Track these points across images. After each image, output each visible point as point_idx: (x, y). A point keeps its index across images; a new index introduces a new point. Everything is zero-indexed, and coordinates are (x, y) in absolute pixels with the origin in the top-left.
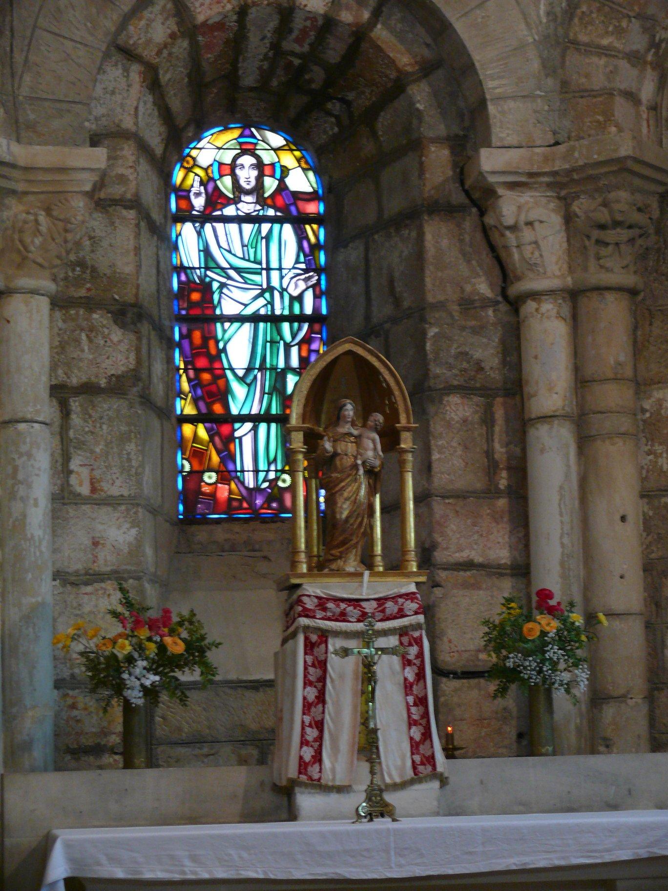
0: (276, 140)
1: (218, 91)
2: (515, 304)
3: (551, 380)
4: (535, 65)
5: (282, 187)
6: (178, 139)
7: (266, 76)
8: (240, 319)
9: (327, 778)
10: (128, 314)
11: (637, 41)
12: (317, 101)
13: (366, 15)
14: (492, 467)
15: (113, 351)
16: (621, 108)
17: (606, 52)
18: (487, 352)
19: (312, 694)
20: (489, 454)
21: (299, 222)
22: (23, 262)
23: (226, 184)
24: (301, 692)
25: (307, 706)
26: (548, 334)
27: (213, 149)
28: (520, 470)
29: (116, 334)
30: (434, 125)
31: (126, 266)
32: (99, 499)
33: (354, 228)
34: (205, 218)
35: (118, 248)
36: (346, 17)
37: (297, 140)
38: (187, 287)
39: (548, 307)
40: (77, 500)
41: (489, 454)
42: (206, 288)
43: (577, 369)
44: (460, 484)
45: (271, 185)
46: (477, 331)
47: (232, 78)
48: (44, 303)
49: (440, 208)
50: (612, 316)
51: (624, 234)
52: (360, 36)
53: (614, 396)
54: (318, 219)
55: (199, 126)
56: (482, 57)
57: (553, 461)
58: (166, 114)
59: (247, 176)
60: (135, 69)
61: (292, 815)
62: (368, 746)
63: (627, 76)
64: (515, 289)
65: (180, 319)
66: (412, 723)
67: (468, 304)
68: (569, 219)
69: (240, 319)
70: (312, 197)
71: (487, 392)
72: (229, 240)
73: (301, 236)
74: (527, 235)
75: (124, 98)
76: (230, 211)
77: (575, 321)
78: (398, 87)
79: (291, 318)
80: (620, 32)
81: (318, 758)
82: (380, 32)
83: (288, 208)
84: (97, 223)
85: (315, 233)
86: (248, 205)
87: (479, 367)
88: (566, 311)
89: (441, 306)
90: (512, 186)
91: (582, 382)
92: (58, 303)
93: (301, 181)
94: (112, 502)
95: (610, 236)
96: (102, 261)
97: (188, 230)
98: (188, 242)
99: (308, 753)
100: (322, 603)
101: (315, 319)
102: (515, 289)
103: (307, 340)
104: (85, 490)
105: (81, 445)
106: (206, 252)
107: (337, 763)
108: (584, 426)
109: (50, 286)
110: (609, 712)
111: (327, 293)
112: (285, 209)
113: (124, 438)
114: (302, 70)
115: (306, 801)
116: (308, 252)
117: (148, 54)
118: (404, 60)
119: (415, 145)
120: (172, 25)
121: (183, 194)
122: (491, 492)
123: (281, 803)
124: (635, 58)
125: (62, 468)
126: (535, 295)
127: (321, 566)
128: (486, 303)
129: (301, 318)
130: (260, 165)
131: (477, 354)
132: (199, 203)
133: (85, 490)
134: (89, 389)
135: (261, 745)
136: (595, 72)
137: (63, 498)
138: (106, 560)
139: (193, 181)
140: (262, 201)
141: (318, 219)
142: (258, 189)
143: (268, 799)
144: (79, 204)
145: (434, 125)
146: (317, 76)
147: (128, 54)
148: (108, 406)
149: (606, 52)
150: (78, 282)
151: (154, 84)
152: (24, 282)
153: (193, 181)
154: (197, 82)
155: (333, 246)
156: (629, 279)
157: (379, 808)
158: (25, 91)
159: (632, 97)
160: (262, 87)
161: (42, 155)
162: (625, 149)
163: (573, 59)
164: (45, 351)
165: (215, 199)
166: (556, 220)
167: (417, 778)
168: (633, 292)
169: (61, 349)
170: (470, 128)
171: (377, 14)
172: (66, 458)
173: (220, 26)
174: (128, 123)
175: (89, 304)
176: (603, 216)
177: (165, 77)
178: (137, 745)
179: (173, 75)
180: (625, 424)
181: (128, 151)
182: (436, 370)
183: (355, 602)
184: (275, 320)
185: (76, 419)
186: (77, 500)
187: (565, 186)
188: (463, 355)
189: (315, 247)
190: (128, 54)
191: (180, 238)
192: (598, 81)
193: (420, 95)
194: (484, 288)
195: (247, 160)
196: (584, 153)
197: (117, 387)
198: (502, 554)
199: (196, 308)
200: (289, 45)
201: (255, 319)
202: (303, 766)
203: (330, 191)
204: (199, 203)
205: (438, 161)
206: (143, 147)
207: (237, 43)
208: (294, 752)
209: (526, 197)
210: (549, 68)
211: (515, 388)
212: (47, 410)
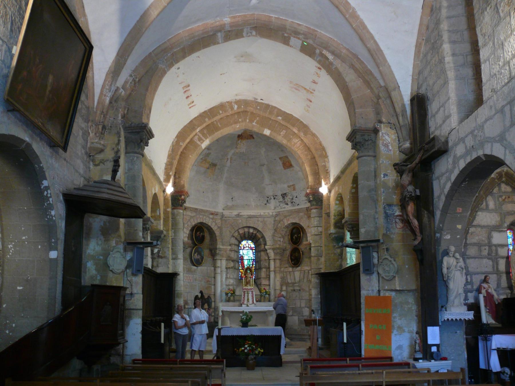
6: (240, 242)
10: (233, 261)
11: (280, 236)
15: (232, 264)
16: (279, 243)
18: (267, 264)
21: (252, 250)
22: (223, 257)
24: (243, 296)
26: (272, 263)
27: (244, 243)
28: (269, 275)
32: (230, 278)
33: (258, 250)
35: (233, 255)
37: (252, 242)
49: (263, 251)
50: (278, 262)
52: (256, 234)
53: (277, 269)
56: (266, 237)
57: (272, 275)
58: (238, 241)
62: (248, 300)
63: (279, 239)
67: (265, 260)
75: (233, 241)
77: (275, 262)
78: (259, 239)
82: (257, 234)
83: (251, 249)
84: (230, 252)
85: (254, 251)
86: (247, 248)
91: (275, 268)
92: (226, 260)
93: (253, 246)
98: (241, 252)
107: (246, 302)
108: (275, 271)
119: (261, 244)
122: (267, 278)
124: (280, 237)
125: (227, 275)
127: (246, 285)
134: (229, 268)
135: (240, 301)
136: (276, 239)
137: (227, 278)
138: (230, 284)
139: (242, 246)
147: (234, 237)
148: (231, 269)
151: (236, 239)
153: (242, 246)
154: (241, 237)
155: (255, 252)
157: (248, 306)
161: (225, 247)
165: (244, 248)
169: (227, 264)
170: (265, 244)
178: (228, 300)
181: (233, 246)
187: (274, 249)
190: (234, 237)
191: (442, 109)
193: (261, 240)
194: (267, 258)
196: (275, 247)
197: (232, 268)
199: (242, 259)
205: (263, 246)
206: (235, 245)
208: (242, 301)
210: (273, 238)
211: (269, 268)
212: (225, 270)
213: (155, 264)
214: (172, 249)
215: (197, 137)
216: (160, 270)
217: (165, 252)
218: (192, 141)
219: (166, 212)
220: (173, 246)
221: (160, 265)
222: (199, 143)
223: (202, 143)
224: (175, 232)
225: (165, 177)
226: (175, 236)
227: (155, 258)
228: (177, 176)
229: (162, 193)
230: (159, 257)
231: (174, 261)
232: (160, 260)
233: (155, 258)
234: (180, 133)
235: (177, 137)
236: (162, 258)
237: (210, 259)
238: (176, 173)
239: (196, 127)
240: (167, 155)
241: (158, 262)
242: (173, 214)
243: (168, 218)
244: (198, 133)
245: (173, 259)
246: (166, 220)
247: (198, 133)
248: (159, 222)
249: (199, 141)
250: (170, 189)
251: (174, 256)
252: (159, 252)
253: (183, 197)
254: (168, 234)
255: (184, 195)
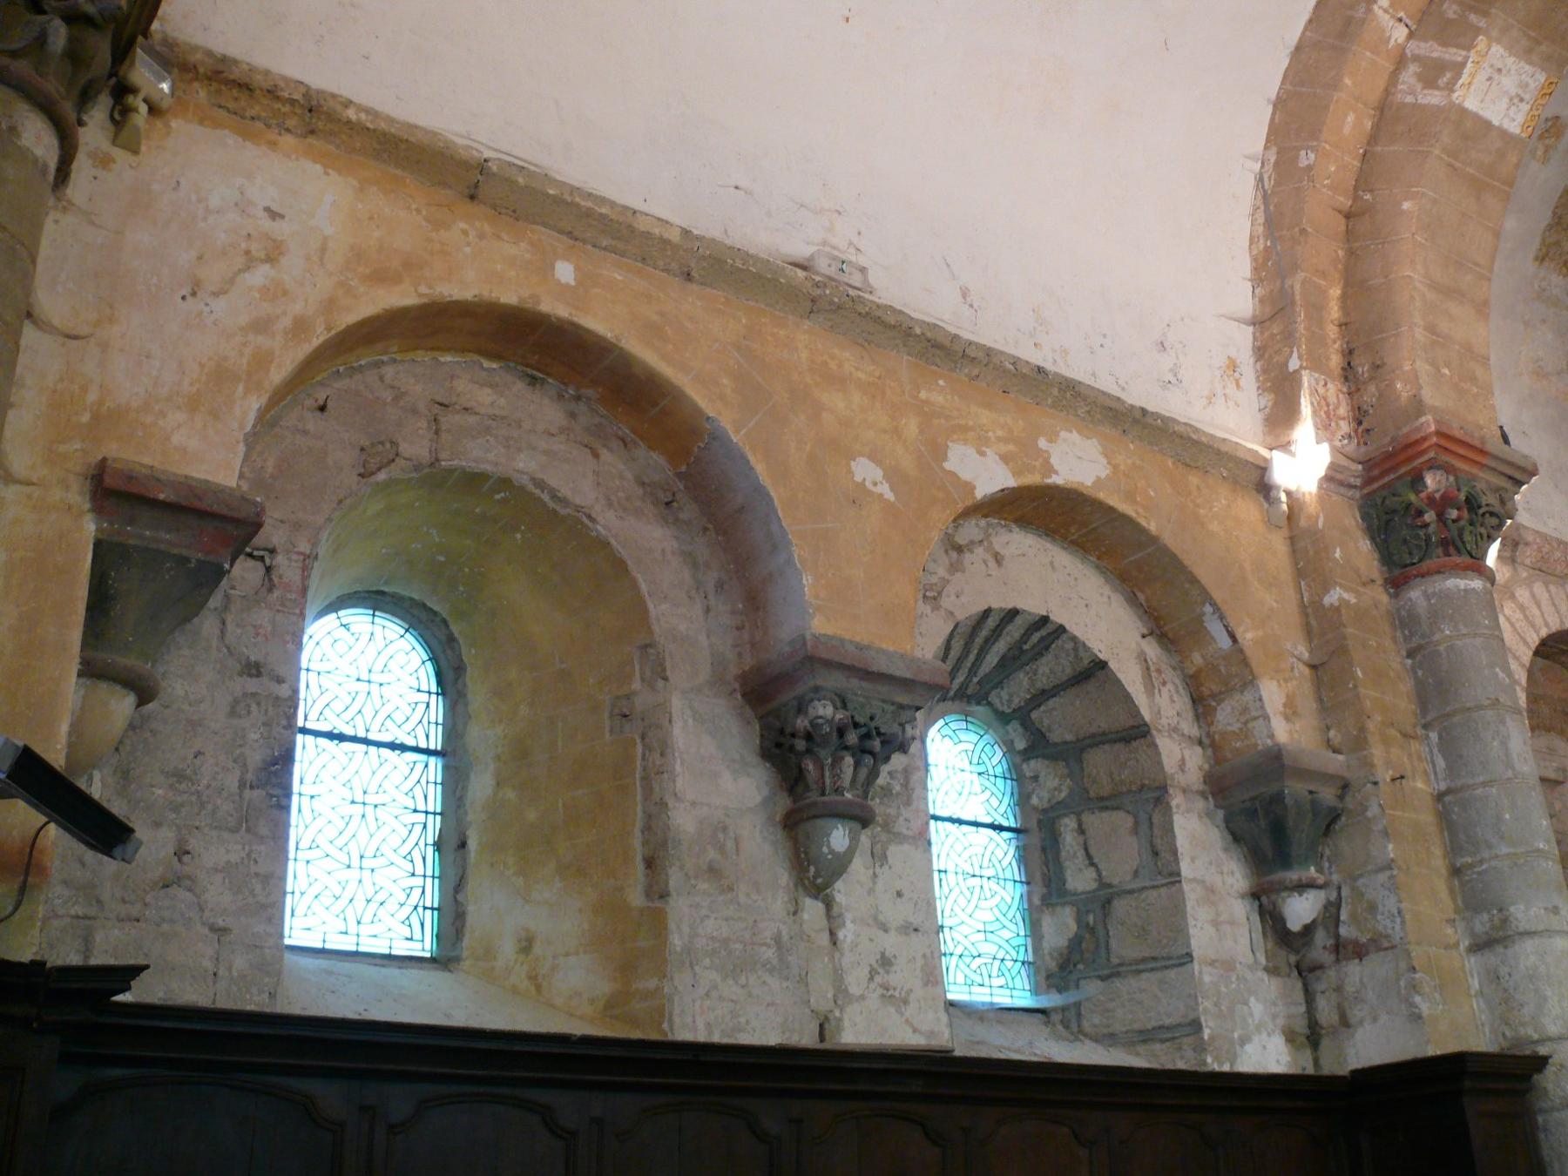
53: (827, 249)
213: (1326, 1011)
214: (1456, 871)
215: (1409, 76)
216: (1372, 1045)
217: (1372, 908)
218: (1388, 116)
219: (1320, 625)
220: (1454, 848)
221: (1356, 1014)
222: (1433, 98)
223: (1450, 87)
224: (1448, 746)
225: (1267, 400)
226: (1451, 770)
227: (1318, 967)
228: (1363, 369)
229: (1248, 509)
230: (1340, 949)
231: (1491, 958)
232: (1354, 972)
233: (1318, 967)
234: (1279, 104)
235: (1276, 134)
236: (1359, 951)
237: (1069, 671)
238: (1349, 353)
239: (1360, 12)
240: (1246, 267)
241: (1339, 989)
242: (1405, 622)
243: (1341, 650)
244: (1414, 47)
245: (1481, 945)
246: (1328, 672)
247: (1414, 47)
248: (1248, 696)
249: (1429, 82)
250: (1304, 464)
251: (1482, 923)
252: (1331, 912)
253: (1431, 481)
254: (1368, 764)
255: (1432, 466)
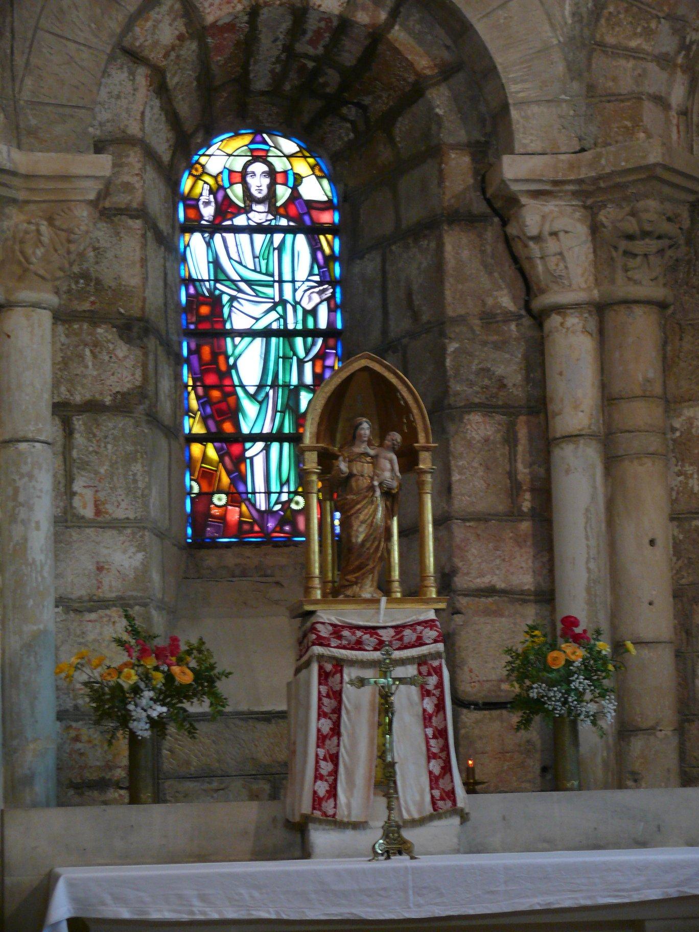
0: (289, 146)
1: (228, 95)
2: (539, 318)
3: (576, 397)
4: (560, 68)
5: (295, 195)
6: (187, 146)
7: (278, 80)
8: (252, 334)
9: (342, 814)
10: (134, 329)
11: (666, 43)
12: (332, 106)
13: (383, 16)
14: (515, 489)
15: (118, 368)
17: (634, 54)
18: (509, 368)
19: (326, 725)
20: (512, 474)
21: (313, 232)
22: (24, 274)
23: (236, 193)
24: (315, 724)
25: (322, 739)
26: (574, 349)
27: (223, 155)
28: (544, 492)
29: (122, 350)
30: (454, 131)
31: (131, 278)
32: (104, 522)
33: (371, 238)
34: (214, 228)
35: (124, 259)
36: (362, 18)
37: (311, 146)
38: (195, 300)
39: (573, 321)
40: (81, 523)
41: (512, 474)
42: (215, 301)
43: (604, 386)
44: (482, 507)
45: (283, 194)
46: (499, 346)
47: (242, 81)
48: (46, 317)
49: (461, 218)
50: (641, 331)
51: (653, 245)
52: (376, 37)
53: (642, 414)
54: (332, 230)
55: (209, 132)
56: (504, 59)
57: (579, 482)
58: (174, 119)
59: (259, 184)
60: (142, 72)
61: (305, 852)
62: (385, 780)
63: (656, 79)
64: (539, 303)
65: (189, 334)
66: (431, 756)
67: (490, 318)
68: (595, 229)
69: (252, 334)
70: (327, 206)
71: (510, 410)
72: (239, 251)
73: (315, 247)
74: (552, 246)
75: (130, 103)
76: (240, 220)
77: (602, 336)
78: (416, 91)
79: (305, 333)
80: (648, 33)
81: (332, 793)
82: (398, 34)
83: (302, 218)
84: (102, 233)
85: (329, 244)
86: (259, 215)
87: (502, 384)
88: (592, 325)
89: (461, 320)
90: (536, 194)
91: (609, 399)
92: (60, 317)
93: (315, 189)
94: (117, 525)
95: (639, 246)
96: (107, 273)
97: (196, 241)
98: (197, 253)
99: (322, 788)
100: (337, 630)
101: (330, 333)
102: (539, 303)
103: (321, 356)
104: (89, 513)
105: (85, 465)
106: (216, 263)
107: (352, 798)
108: (611, 446)
109: (52, 299)
110: (637, 745)
111: (343, 307)
112: (298, 219)
113: (130, 459)
114: (316, 73)
115: (320, 837)
116: (322, 263)
117: (155, 56)
118: (423, 63)
119: (434, 152)
120: (180, 26)
121: (192, 203)
122: (513, 515)
123: (294, 840)
124: (664, 61)
125: (65, 490)
126: (560, 309)
127: (336, 592)
128: (509, 317)
129: (315, 333)
130: (272, 173)
131: (500, 371)
132: (208, 212)
133: (89, 513)
134: (93, 407)
135: (273, 779)
136: (622, 75)
137: (66, 521)
138: (111, 586)
139: (202, 190)
140: (274, 210)
141: (332, 230)
142: (270, 197)
143: (280, 835)
144: (83, 213)
145: (454, 131)
146: (331, 79)
147: (134, 56)
148: (113, 425)
149: (634, 54)
150: (82, 295)
152: (26, 295)
153: (202, 190)
154: (206, 86)
155: (348, 257)
156: (658, 292)
157: (396, 845)
158: (26, 95)
159: (661, 101)
160: (275, 91)
161: (44, 162)
162: (655, 156)
163: (600, 62)
164: (47, 367)
165: (225, 208)
166: (582, 230)
167: (437, 814)
168: (662, 306)
169: (64, 365)
170: (492, 133)
171: (394, 14)
172: (69, 479)
173: (230, 27)
174: (134, 129)
175: (93, 318)
176: (631, 226)
177: (172, 81)
178: (144, 779)
179: (181, 78)
180: (654, 443)
182: (456, 387)
183: (372, 630)
184: (288, 335)
185: (79, 439)
186: (81, 523)
187: (591, 194)
188: (485, 371)
189: (330, 259)
190: (134, 56)
191: (188, 249)
192: (626, 85)
193: (440, 99)
194: (506, 301)
195: (259, 168)
196: (611, 160)
197: (123, 404)
198: (525, 580)
199: (206, 322)
200: (302, 47)
201: (267, 333)
202: (317, 801)
203: (346, 200)
204: (208, 212)
205: (458, 168)
206: (150, 154)
207: (248, 45)
208: (307, 786)
209: (551, 206)
210: (575, 72)
211: (539, 406)
212: (50, 429)
